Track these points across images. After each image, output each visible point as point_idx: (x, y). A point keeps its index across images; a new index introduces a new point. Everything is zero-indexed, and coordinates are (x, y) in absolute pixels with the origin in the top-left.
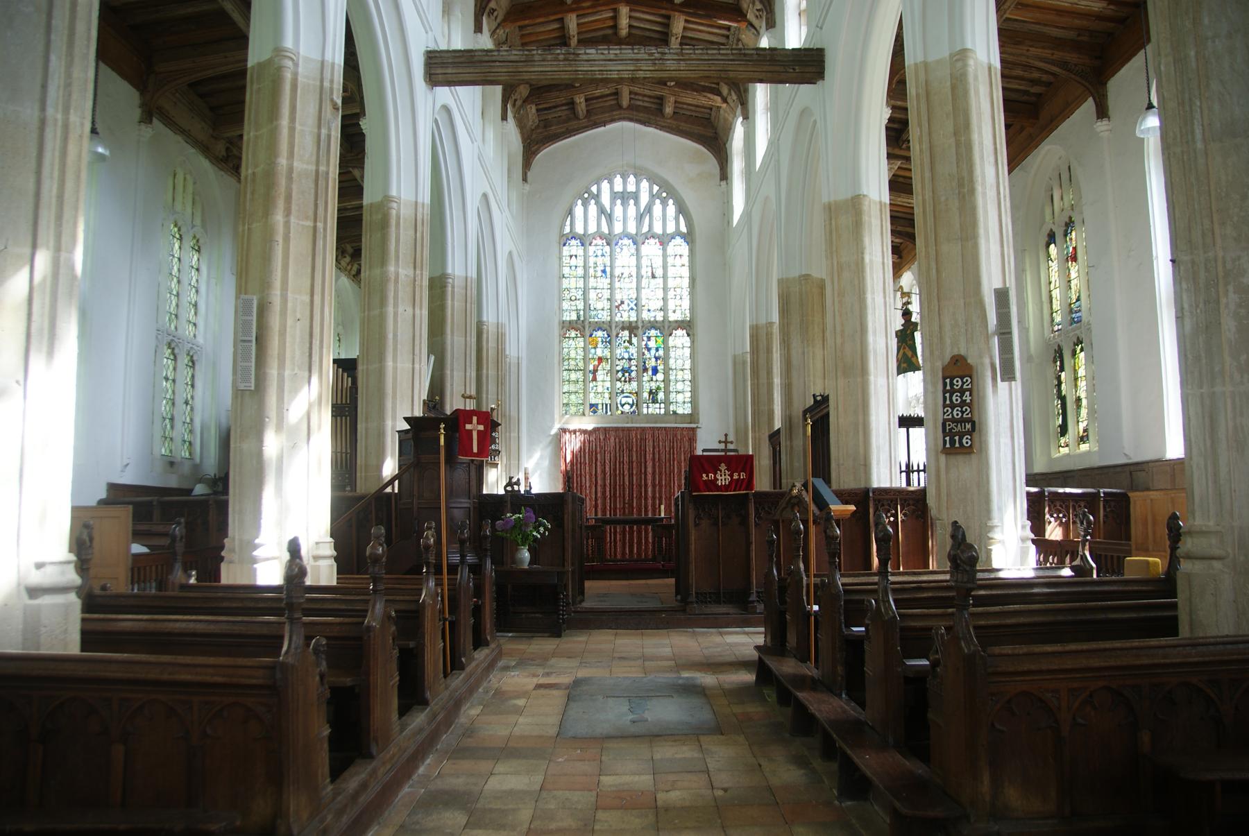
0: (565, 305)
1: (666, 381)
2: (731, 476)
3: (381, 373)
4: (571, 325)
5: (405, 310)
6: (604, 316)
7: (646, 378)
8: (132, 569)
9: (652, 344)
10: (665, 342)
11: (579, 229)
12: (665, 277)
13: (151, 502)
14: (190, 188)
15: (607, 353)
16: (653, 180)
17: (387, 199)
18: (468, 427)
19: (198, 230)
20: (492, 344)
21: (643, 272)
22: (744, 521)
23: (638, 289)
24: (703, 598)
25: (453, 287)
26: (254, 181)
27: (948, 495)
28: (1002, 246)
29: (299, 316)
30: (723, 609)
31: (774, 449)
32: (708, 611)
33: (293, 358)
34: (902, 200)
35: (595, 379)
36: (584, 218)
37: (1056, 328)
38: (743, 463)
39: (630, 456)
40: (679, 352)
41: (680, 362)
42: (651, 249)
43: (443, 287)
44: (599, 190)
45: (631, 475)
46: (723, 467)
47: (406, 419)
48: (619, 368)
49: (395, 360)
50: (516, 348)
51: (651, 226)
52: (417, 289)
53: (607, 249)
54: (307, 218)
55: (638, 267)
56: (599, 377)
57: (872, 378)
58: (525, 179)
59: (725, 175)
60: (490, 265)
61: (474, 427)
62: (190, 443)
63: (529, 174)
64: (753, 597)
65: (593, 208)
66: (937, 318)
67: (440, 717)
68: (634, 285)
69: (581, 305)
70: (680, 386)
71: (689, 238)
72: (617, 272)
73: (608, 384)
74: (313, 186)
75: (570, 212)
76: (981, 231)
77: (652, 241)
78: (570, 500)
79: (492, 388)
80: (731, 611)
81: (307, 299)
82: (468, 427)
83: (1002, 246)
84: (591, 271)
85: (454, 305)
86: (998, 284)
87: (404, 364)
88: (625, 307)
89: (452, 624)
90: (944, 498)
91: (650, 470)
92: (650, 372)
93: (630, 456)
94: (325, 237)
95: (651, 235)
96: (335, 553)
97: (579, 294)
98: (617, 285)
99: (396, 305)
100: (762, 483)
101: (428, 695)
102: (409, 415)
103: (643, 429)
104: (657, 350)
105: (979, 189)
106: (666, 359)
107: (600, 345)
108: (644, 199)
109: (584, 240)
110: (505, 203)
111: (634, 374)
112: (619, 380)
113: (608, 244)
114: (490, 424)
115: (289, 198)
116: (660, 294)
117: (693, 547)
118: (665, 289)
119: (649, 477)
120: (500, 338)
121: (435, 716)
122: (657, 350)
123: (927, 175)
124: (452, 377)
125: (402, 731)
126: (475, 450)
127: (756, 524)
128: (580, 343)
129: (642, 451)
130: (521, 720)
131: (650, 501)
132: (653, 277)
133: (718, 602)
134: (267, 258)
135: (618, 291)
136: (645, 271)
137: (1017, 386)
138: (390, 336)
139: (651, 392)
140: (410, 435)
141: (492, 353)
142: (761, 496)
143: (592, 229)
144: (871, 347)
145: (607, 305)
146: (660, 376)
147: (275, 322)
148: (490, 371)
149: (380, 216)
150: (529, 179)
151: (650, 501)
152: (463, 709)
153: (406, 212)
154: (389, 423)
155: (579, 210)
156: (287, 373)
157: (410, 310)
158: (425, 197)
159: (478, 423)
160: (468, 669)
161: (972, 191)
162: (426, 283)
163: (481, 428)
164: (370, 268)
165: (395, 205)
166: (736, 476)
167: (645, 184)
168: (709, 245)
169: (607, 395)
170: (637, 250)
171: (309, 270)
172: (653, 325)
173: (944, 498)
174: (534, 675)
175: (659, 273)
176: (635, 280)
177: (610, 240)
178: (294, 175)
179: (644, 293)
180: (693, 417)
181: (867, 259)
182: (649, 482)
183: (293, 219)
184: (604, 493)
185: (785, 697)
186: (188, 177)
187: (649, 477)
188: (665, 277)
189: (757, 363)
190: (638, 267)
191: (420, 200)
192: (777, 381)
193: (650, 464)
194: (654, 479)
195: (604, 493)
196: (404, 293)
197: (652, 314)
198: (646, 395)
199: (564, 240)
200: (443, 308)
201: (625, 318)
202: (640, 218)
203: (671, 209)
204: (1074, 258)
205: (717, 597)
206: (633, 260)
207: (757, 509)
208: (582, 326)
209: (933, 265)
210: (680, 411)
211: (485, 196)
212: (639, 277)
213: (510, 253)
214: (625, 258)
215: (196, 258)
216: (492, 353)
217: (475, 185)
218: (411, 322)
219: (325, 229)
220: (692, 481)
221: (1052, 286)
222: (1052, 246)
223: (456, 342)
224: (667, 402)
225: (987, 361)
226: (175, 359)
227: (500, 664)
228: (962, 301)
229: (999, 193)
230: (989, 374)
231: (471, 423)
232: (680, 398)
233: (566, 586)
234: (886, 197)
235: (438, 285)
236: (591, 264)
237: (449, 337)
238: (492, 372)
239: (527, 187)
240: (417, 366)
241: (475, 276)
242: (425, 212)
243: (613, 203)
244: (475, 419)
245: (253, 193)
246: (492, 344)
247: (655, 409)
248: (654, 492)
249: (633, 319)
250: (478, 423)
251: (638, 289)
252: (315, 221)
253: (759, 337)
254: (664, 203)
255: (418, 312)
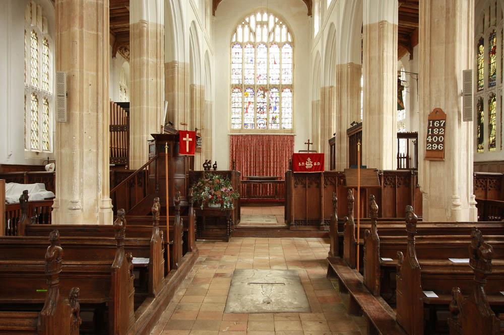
0: (233, 76)
1: (280, 113)
2: (313, 164)
3: (141, 110)
4: (236, 87)
5: (152, 79)
6: (251, 82)
7: (271, 111)
8: (6, 212)
9: (274, 95)
10: (280, 95)
11: (240, 40)
12: (280, 63)
13: (23, 174)
14: (40, 13)
15: (252, 100)
16: (275, 15)
17: (142, 22)
18: (184, 139)
19: (48, 37)
20: (198, 95)
21: (270, 61)
22: (319, 186)
23: (268, 69)
24: (298, 222)
25: (178, 68)
26: (62, 7)
27: (430, 180)
28: (468, 47)
29: (90, 83)
30: (308, 228)
31: (331, 146)
32: (301, 229)
33: (88, 105)
34: (407, 25)
35: (247, 112)
36: (243, 34)
37: (480, 89)
38: (319, 157)
39: (263, 148)
40: (287, 99)
41: (287, 105)
42: (274, 49)
43: (173, 67)
44: (249, 20)
45: (263, 157)
46: (309, 159)
47: (152, 135)
48: (258, 107)
49: (147, 105)
50: (210, 97)
51: (274, 38)
52: (158, 68)
53: (253, 49)
54: (93, 29)
55: (268, 59)
56: (249, 110)
57: (385, 116)
58: (214, 14)
59: (310, 13)
60: (197, 56)
61: (188, 139)
62: (47, 143)
63: (216, 12)
64: (323, 223)
65: (246, 29)
66: (428, 87)
67: (161, 302)
68: (266, 67)
69: (241, 77)
70: (287, 116)
71: (292, 44)
72: (258, 61)
73: (253, 114)
74: (95, 12)
75: (235, 31)
76: (458, 38)
77: (274, 46)
78: (234, 173)
79: (198, 116)
80: (312, 229)
81: (94, 73)
82: (184, 139)
83: (468, 47)
84: (246, 60)
85: (178, 77)
86: (464, 68)
87: (152, 107)
88: (261, 78)
89: (171, 246)
90: (428, 182)
91: (272, 154)
92: (273, 109)
93: (263, 148)
94: (103, 40)
95: (274, 43)
96: (112, 206)
97: (240, 71)
98: (258, 67)
99: (147, 77)
100: (327, 168)
101: (154, 292)
102: (154, 133)
103: (269, 136)
104: (276, 98)
105: (458, 14)
106: (280, 103)
107: (249, 95)
108: (271, 25)
109: (242, 45)
110: (203, 27)
111: (265, 110)
112: (259, 113)
113: (254, 47)
114: (195, 136)
115: (81, 18)
116: (278, 71)
117: (293, 198)
118: (281, 69)
119: (272, 158)
120: (202, 93)
121: (158, 303)
122: (276, 98)
123: (428, 6)
124: (178, 112)
125: (136, 317)
126: (188, 150)
127: (325, 187)
128: (240, 94)
129: (268, 146)
130: (206, 300)
131: (272, 169)
132: (275, 63)
133: (306, 225)
134: (71, 50)
135: (258, 70)
136: (272, 61)
137: (473, 122)
138: (145, 92)
139: (273, 118)
140: (154, 142)
141: (198, 99)
142: (326, 173)
143: (246, 40)
144: (385, 100)
145: (253, 77)
146: (277, 111)
147: (77, 86)
148: (197, 108)
149: (138, 31)
150: (216, 15)
151: (272, 169)
152: (176, 292)
153: (151, 29)
154: (145, 136)
155: (240, 30)
156: (85, 113)
157: (155, 80)
158: (161, 21)
159: (189, 137)
160: (180, 269)
161: (454, 15)
162: (163, 65)
163: (191, 140)
164: (134, 58)
165: (145, 25)
166: (315, 164)
167: (272, 17)
168: (301, 42)
169: (253, 120)
170: (268, 50)
171: (95, 58)
172: (274, 87)
173: (428, 182)
174: (214, 268)
175: (278, 61)
176: (266, 65)
177: (254, 45)
178: (84, 5)
179: (271, 71)
180: (292, 131)
181: (385, 54)
182: (272, 161)
183: (84, 30)
184: (250, 165)
185: (343, 288)
186: (39, 6)
187: (272, 158)
188: (280, 63)
189: (323, 107)
190: (268, 59)
191: (159, 23)
192: (334, 114)
193: (272, 152)
194: (274, 159)
195: (250, 165)
196: (151, 71)
197: (274, 81)
198: (270, 120)
199: (233, 45)
200: (173, 78)
201: (261, 83)
202: (269, 34)
203: (284, 29)
204: (494, 52)
205: (305, 222)
206: (265, 56)
207: (325, 180)
208: (240, 87)
209: (428, 58)
210: (287, 127)
211: (193, 22)
212: (268, 63)
213: (207, 51)
214: (262, 51)
215: (46, 50)
216: (198, 99)
217: (188, 16)
218: (155, 85)
219: (103, 36)
220: (293, 165)
221: (480, 67)
222: (481, 46)
223: (180, 95)
224: (281, 123)
225: (456, 110)
226: (37, 101)
227: (198, 259)
228: (443, 78)
229: (468, 16)
230: (457, 117)
231: (186, 137)
232: (287, 121)
233: (231, 217)
234: (396, 22)
235: (170, 67)
236: (246, 57)
237: (176, 92)
238: (198, 109)
239: (215, 18)
240: (159, 108)
241: (189, 62)
242: (161, 29)
243: (256, 27)
244: (188, 135)
245: (62, 14)
246: (198, 95)
247: (274, 127)
248: (274, 165)
249: (265, 83)
250: (189, 137)
251: (268, 69)
252: (97, 31)
253: (325, 94)
254: (281, 26)
255: (159, 80)
